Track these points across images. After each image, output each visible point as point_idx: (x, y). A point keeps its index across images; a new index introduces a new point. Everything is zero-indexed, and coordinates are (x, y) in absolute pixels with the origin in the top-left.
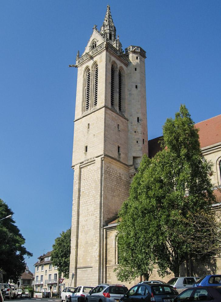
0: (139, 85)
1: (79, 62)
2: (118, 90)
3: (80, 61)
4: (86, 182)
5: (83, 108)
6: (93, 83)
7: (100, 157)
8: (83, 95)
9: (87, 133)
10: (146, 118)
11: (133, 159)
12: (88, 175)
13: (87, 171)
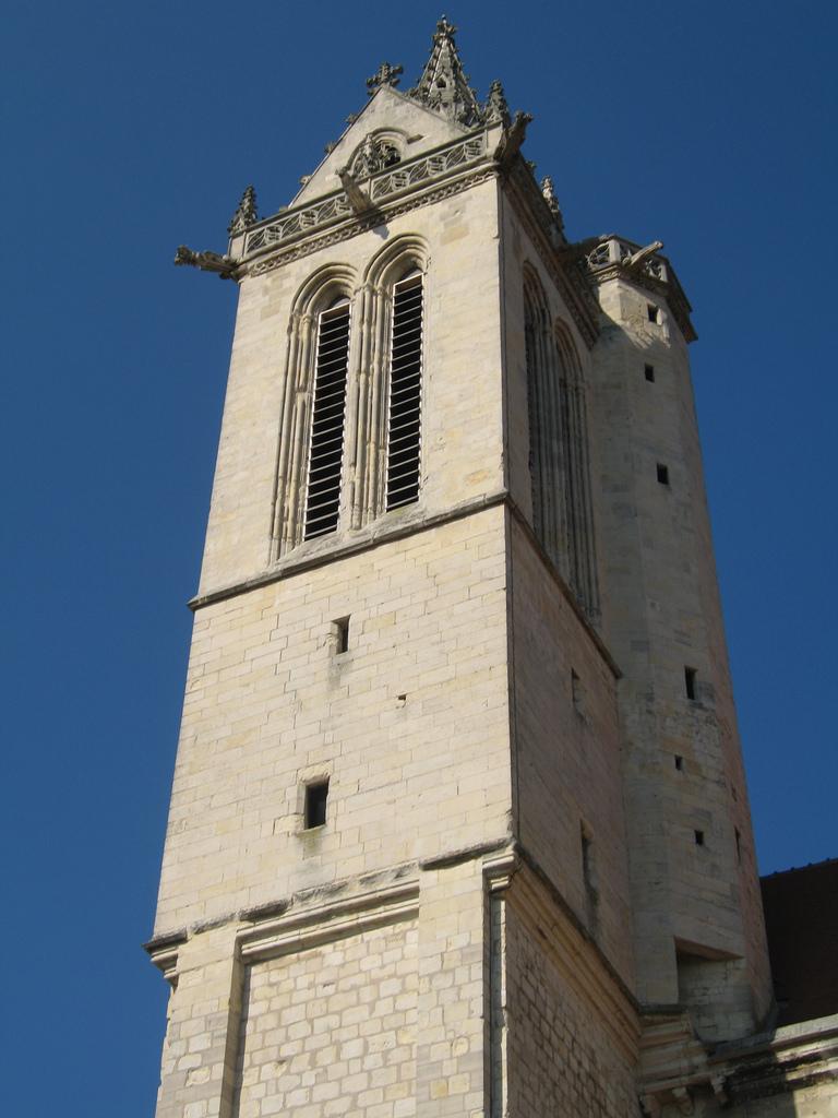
0: (675, 469)
1: (256, 242)
3: (266, 239)
4: (309, 1079)
5: (283, 519)
6: (375, 365)
7: (474, 868)
8: (285, 438)
11: (679, 975)
12: (333, 1020)
13: (311, 986)
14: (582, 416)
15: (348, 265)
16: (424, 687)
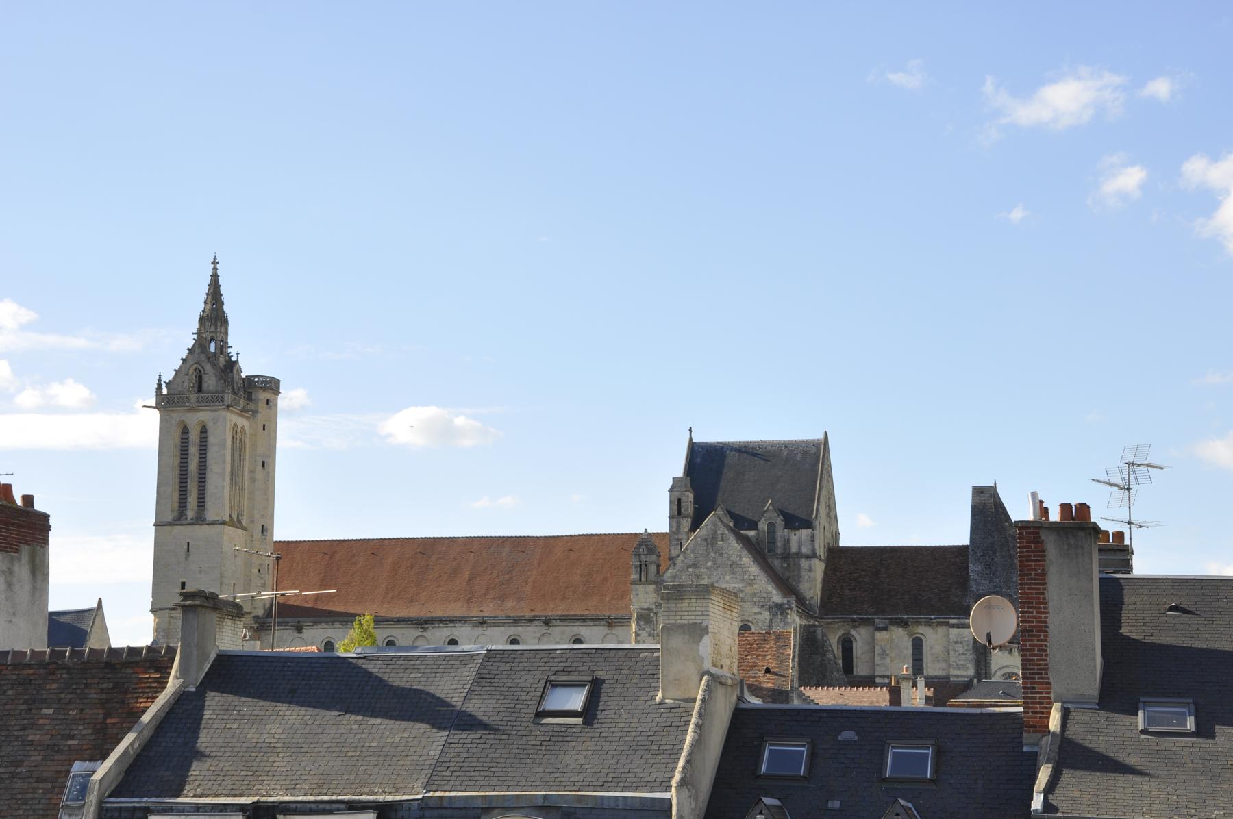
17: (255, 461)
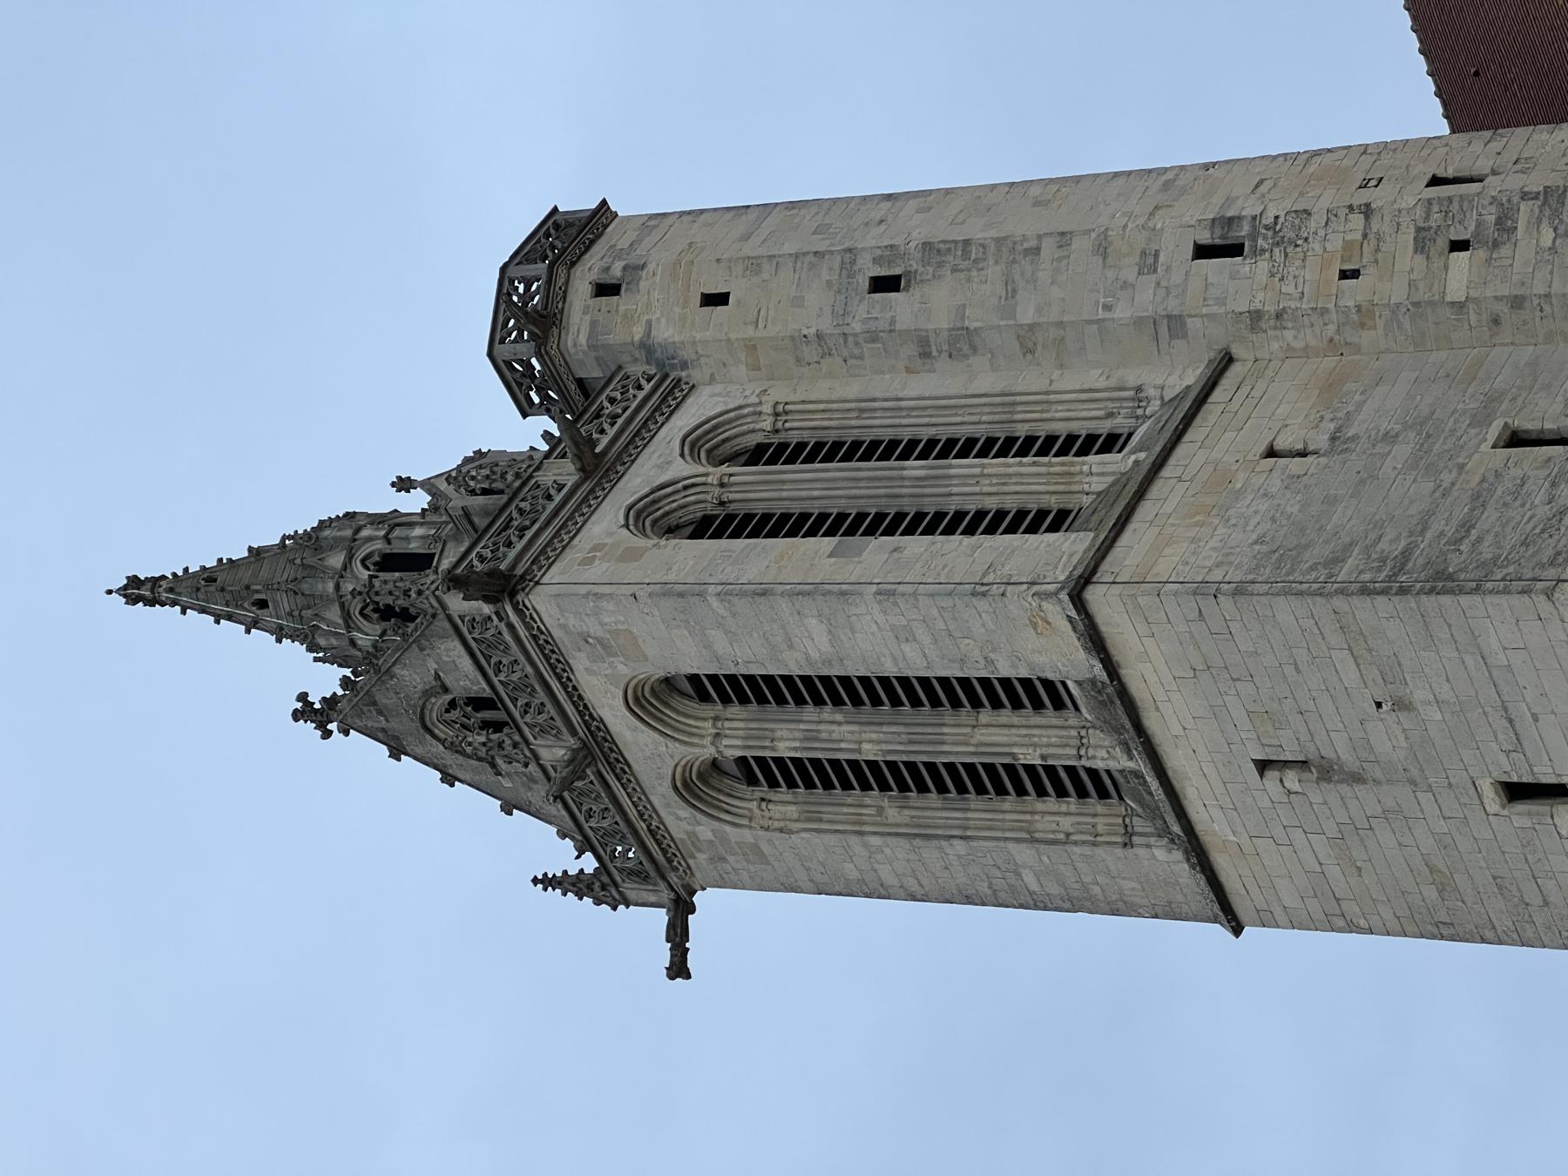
2: (915, 468)
9: (1360, 790)
10: (1207, 167)
14: (821, 406)
15: (676, 766)
16: (1365, 683)
17: (873, 337)
